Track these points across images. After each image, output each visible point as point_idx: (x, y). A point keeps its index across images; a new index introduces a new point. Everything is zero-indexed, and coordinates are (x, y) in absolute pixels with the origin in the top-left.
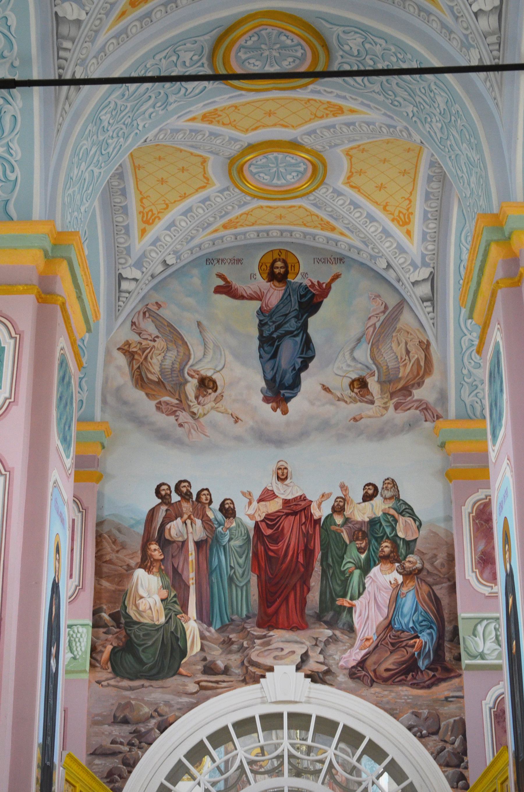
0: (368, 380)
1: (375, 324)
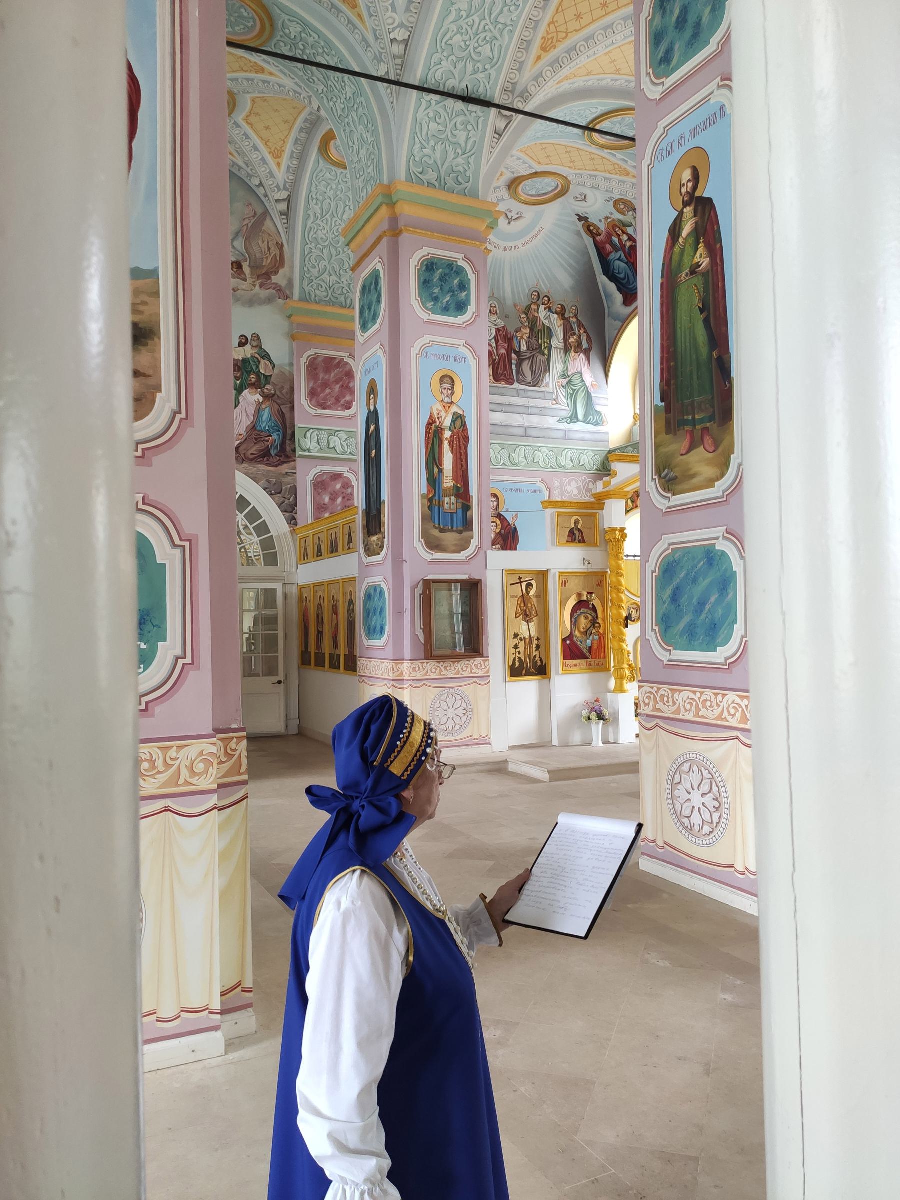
0: (243, 264)
1: (248, 224)
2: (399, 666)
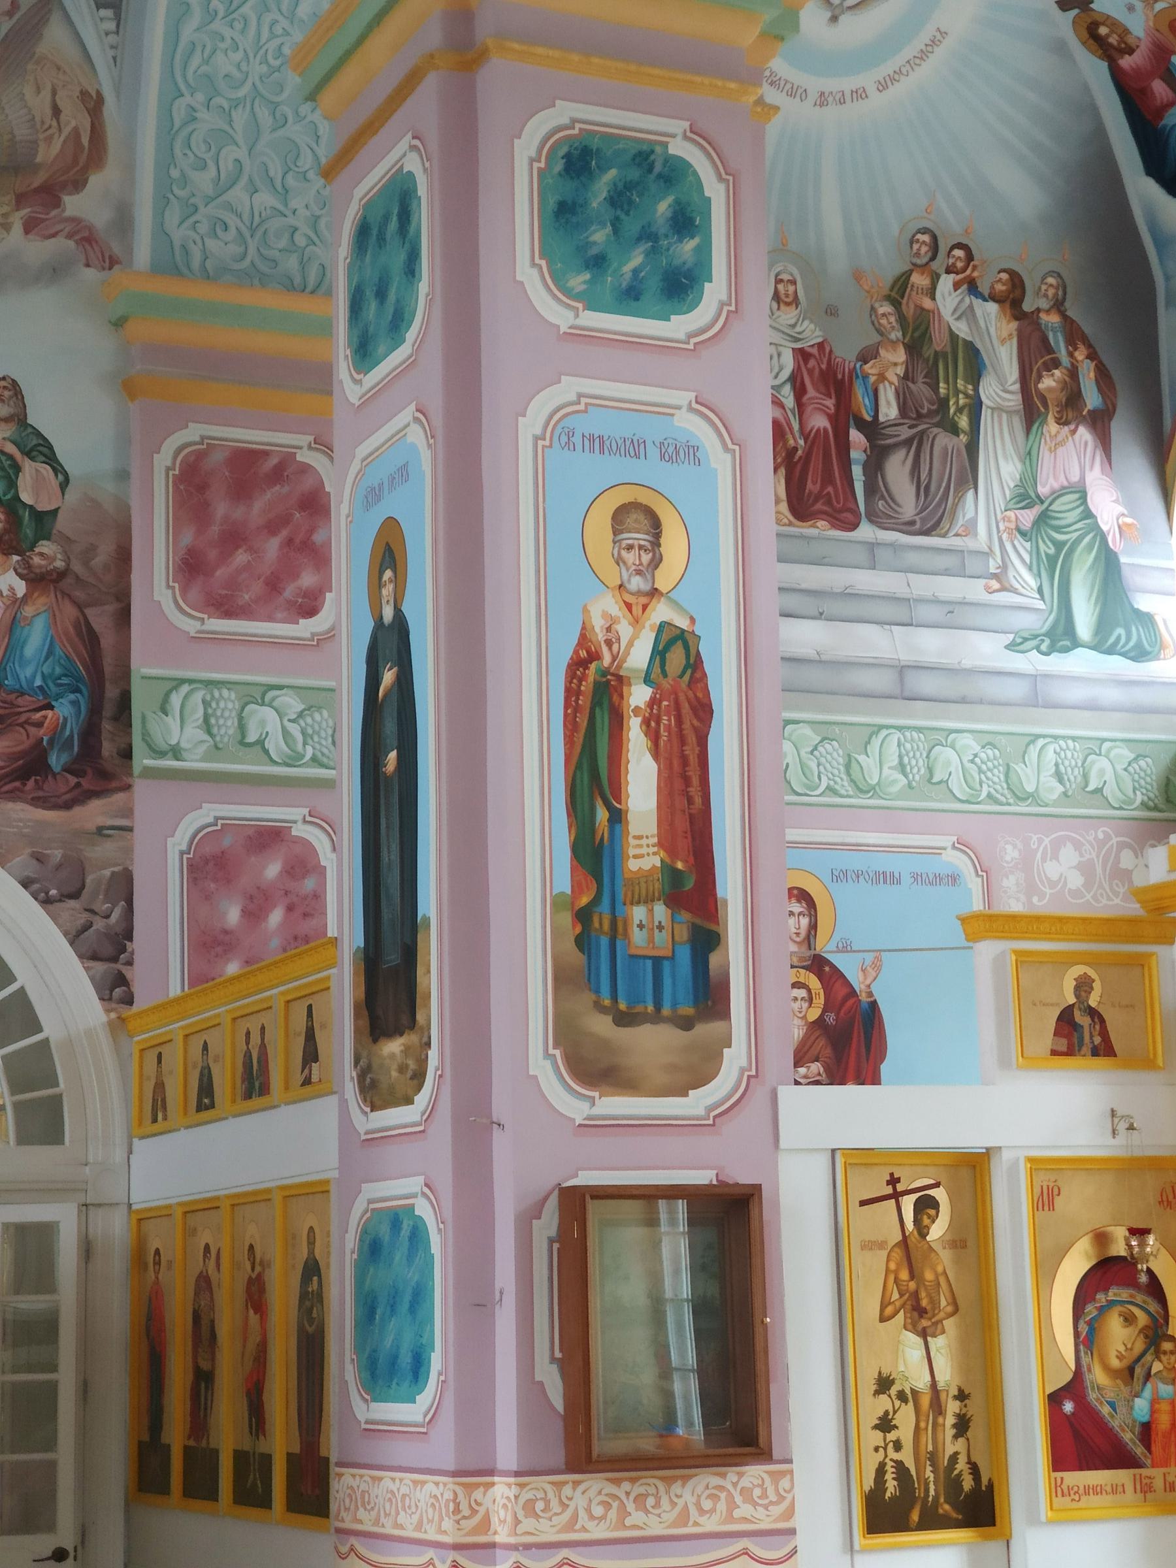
2: (478, 1494)
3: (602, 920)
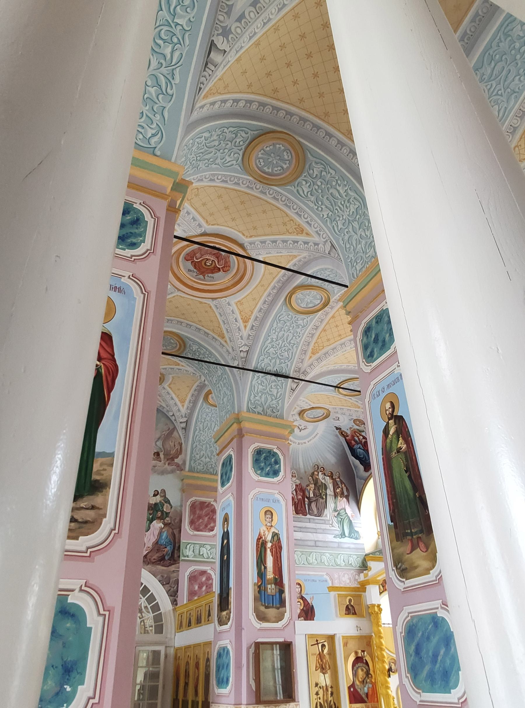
3: (263, 588)
